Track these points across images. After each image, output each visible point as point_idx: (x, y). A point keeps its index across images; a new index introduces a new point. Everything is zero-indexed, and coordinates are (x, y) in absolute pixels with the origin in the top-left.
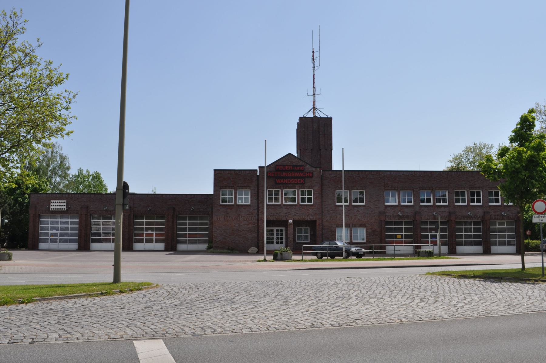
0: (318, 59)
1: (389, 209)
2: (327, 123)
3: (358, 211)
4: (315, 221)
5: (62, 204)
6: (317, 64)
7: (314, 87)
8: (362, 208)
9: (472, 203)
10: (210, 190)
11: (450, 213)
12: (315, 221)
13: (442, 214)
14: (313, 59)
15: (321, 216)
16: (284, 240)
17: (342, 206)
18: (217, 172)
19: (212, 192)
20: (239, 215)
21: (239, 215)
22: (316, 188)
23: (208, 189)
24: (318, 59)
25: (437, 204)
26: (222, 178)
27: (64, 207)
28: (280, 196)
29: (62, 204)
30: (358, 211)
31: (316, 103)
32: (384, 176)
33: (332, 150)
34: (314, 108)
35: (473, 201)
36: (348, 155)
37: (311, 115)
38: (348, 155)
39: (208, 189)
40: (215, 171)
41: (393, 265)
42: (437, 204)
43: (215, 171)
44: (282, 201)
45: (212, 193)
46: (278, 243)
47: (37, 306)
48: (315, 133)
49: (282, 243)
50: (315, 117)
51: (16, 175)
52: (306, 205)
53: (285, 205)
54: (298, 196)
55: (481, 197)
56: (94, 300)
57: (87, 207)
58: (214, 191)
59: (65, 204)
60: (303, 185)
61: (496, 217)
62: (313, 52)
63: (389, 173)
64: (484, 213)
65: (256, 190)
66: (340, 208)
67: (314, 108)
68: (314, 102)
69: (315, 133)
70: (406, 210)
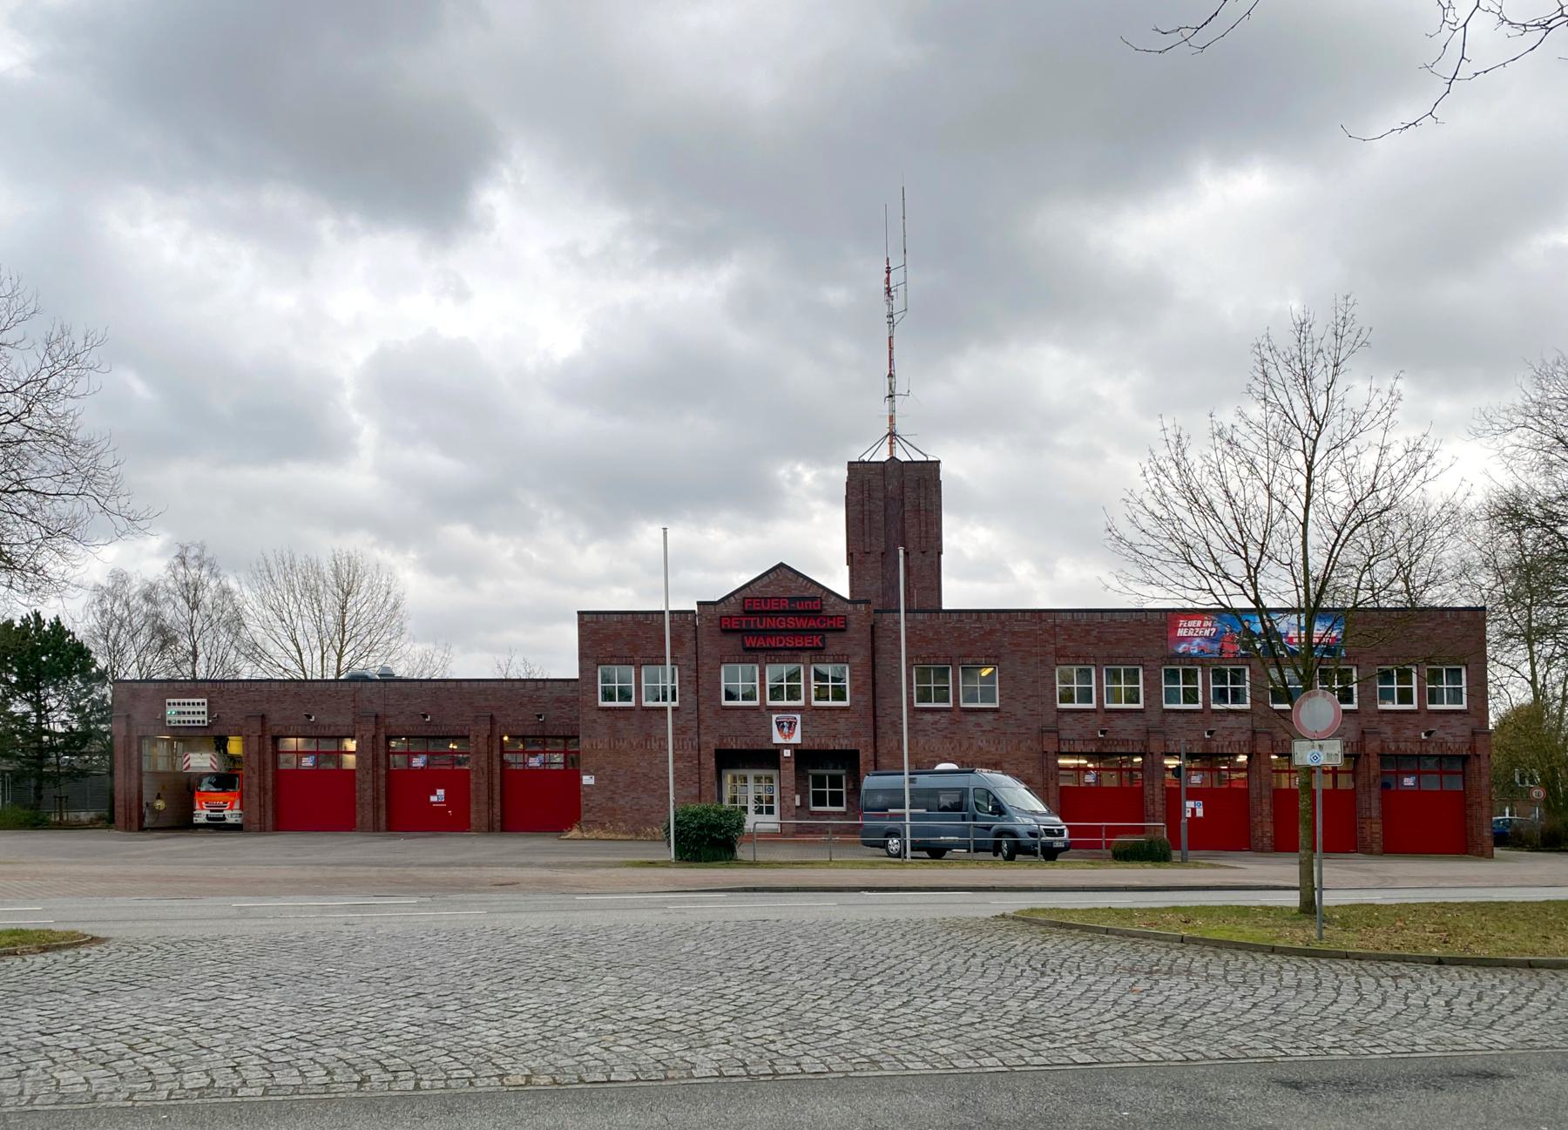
1: (1068, 718)
2: (926, 476)
3: (978, 725)
4: (855, 754)
6: (898, 304)
8: (990, 717)
9: (1432, 702)
11: (1254, 732)
12: (855, 754)
13: (1231, 734)
16: (776, 805)
17: (665, 709)
18: (587, 618)
19: (573, 673)
22: (856, 660)
23: (566, 666)
25: (1431, 707)
26: (604, 635)
30: (978, 725)
31: (897, 421)
34: (892, 434)
36: (983, 566)
38: (983, 566)
39: (566, 666)
41: (1137, 883)
42: (1431, 707)
44: (956, 700)
45: (576, 676)
46: (759, 811)
48: (895, 507)
49: (770, 811)
50: (893, 458)
52: (621, 709)
53: (817, 709)
54: (808, 682)
55: (1141, 686)
56: (1467, 948)
58: (581, 671)
59: (204, 709)
60: (819, 653)
61: (1402, 745)
65: (693, 666)
67: (892, 434)
68: (891, 419)
69: (895, 507)
70: (1120, 723)
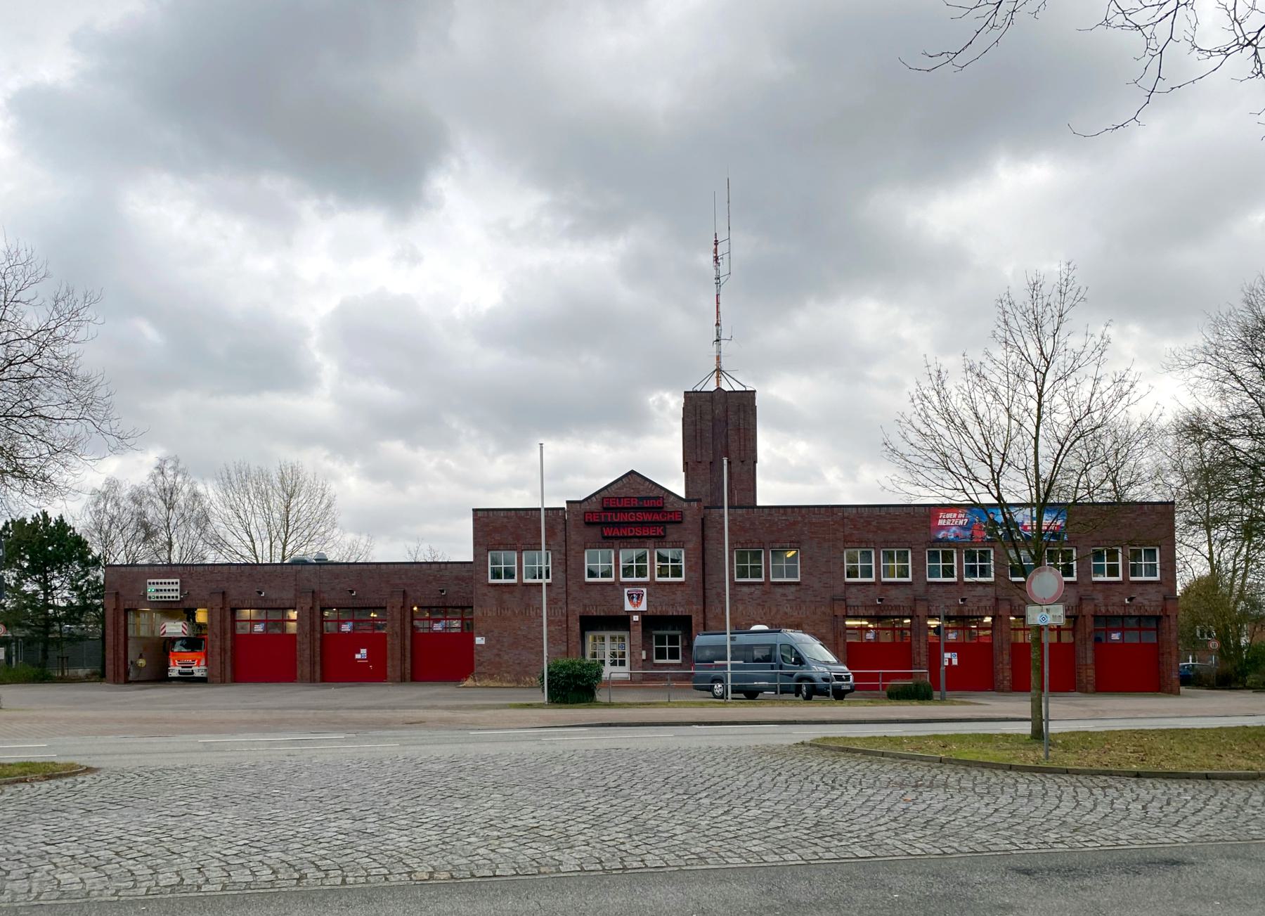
0: (726, 257)
2: (744, 404)
4: (690, 618)
5: (171, 587)
6: (723, 268)
7: (718, 324)
8: (793, 589)
10: (466, 554)
11: (997, 599)
14: (716, 258)
15: (701, 608)
16: (627, 659)
18: (480, 514)
20: (528, 605)
21: (528, 605)
24: (726, 257)
25: (1132, 579)
26: (496, 528)
27: (174, 594)
28: (648, 564)
29: (171, 587)
32: (844, 518)
33: (755, 462)
34: (719, 370)
35: (972, 571)
37: (711, 387)
38: (790, 471)
40: (475, 511)
42: (1132, 579)
43: (475, 511)
44: (767, 576)
46: (614, 664)
47: (935, 799)
48: (721, 427)
49: (622, 663)
51: (52, 524)
53: (659, 583)
54: (652, 563)
57: (224, 593)
58: (475, 556)
59: (177, 587)
60: (661, 540)
62: (716, 243)
63: (854, 510)
64: (1081, 599)
66: (533, 590)
67: (719, 370)
68: (718, 358)
70: (893, 593)
